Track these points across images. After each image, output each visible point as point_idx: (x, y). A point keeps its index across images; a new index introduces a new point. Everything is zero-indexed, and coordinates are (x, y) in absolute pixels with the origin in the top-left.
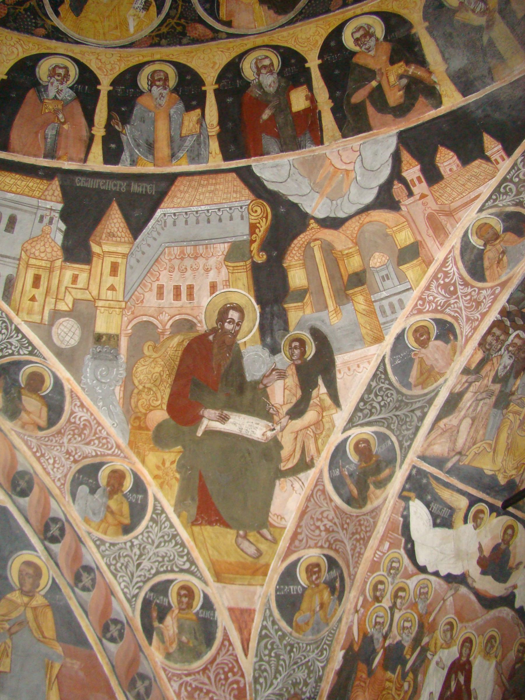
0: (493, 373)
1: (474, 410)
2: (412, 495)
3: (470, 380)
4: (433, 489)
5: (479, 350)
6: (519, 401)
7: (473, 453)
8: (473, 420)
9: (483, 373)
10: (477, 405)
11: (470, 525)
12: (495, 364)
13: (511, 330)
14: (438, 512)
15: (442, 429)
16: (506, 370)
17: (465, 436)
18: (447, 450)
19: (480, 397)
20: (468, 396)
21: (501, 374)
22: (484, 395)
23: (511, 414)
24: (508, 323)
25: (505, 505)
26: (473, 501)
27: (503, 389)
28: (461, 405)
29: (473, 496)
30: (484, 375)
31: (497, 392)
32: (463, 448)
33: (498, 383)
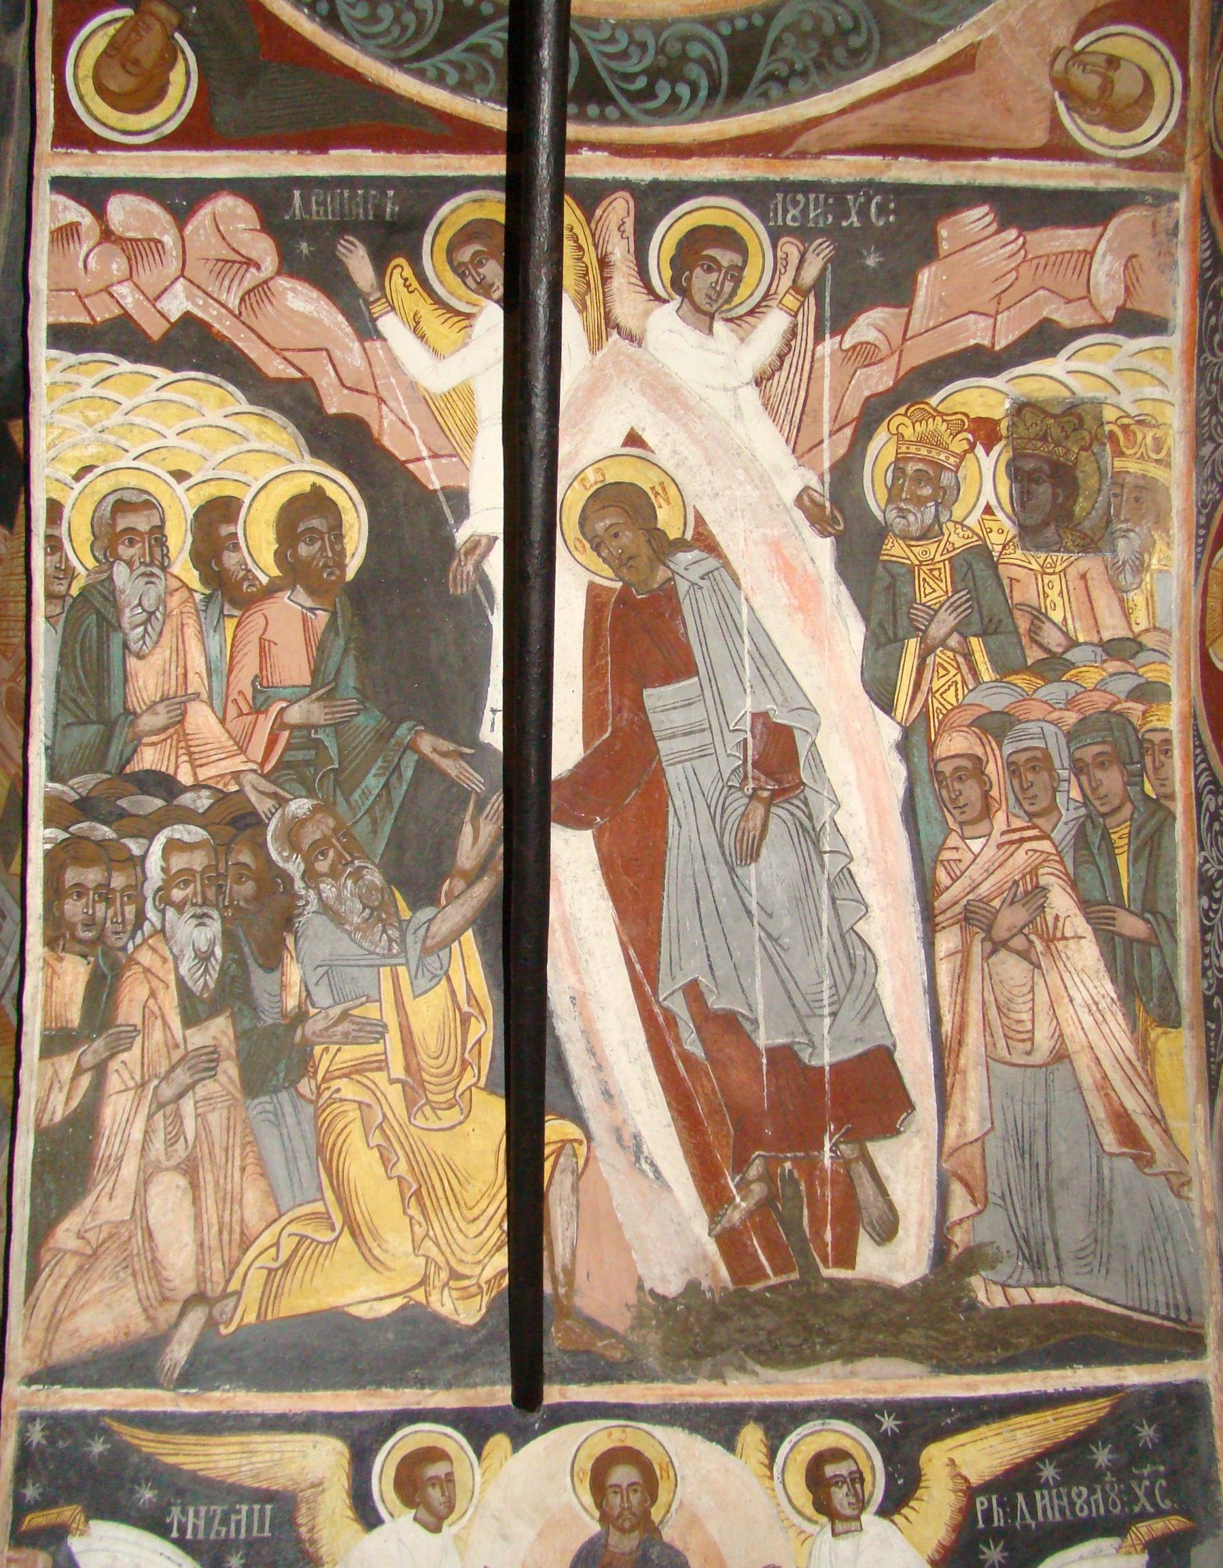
0: (170, 1000)
1: (171, 1142)
2: (67, 1513)
3: (89, 1060)
4: (149, 1459)
5: (61, 959)
6: (345, 1026)
7: (256, 1279)
8: (190, 1169)
9: (129, 1010)
10: (178, 1117)
11: (400, 1524)
12: (157, 966)
13: (135, 847)
14: (218, 1531)
15: (75, 1253)
16: (215, 966)
17: (188, 1237)
18: (137, 1310)
19: (168, 1092)
20: (115, 1108)
21: (203, 982)
22: (182, 1077)
23: (342, 1083)
24: (106, 832)
25: (527, 1393)
26: (363, 1438)
27: (246, 1023)
28: (107, 1147)
29: (353, 1415)
30: (137, 1020)
31: (227, 1044)
32: (201, 1278)
33: (214, 1013)
